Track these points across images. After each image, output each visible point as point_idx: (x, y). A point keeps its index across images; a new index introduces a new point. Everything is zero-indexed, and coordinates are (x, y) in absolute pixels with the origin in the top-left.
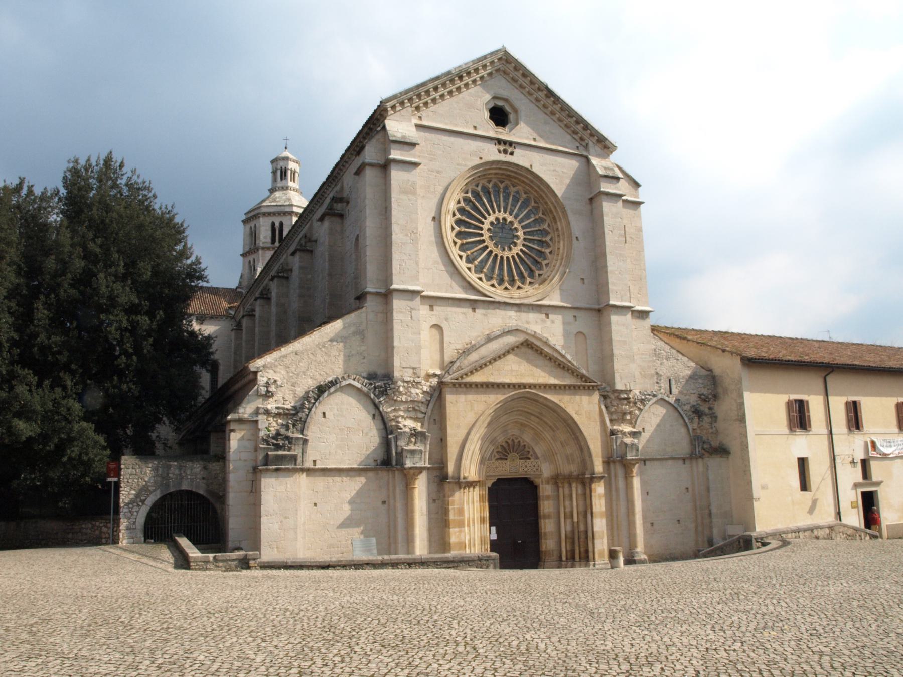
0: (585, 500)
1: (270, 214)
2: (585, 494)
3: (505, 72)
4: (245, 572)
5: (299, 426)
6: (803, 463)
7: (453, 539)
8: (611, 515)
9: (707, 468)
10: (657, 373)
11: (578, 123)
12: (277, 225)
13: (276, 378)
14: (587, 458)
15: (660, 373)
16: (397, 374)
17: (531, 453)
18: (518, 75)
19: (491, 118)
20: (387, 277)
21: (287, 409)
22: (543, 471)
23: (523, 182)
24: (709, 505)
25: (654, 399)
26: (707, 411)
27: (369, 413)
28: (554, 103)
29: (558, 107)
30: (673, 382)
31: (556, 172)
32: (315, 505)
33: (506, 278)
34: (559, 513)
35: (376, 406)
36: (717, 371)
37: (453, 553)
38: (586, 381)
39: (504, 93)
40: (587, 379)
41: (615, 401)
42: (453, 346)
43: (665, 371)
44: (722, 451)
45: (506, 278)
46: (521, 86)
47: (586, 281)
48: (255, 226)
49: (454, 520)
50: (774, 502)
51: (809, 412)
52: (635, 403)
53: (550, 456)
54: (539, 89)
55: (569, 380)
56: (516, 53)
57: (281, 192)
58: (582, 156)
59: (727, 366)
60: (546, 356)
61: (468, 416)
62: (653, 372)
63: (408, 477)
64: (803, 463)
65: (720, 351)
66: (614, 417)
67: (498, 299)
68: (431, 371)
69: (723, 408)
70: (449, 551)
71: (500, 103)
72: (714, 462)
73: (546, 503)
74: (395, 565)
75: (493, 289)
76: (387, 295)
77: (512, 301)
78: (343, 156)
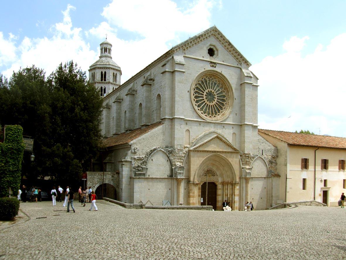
0: (232, 190)
1: (100, 68)
2: (232, 188)
3: (215, 35)
4: (142, 209)
5: (145, 164)
6: (304, 180)
7: (191, 202)
8: (240, 196)
9: (272, 181)
10: (259, 148)
11: (239, 55)
12: (103, 73)
13: (137, 147)
14: (234, 176)
15: (260, 148)
16: (175, 147)
17: (216, 174)
18: (219, 36)
19: (209, 53)
20: (172, 112)
21: (141, 158)
22: (219, 180)
23: (218, 77)
24: (272, 194)
25: (257, 157)
26: (274, 161)
27: (166, 160)
28: (231, 47)
29: (232, 49)
30: (264, 151)
31: (231, 76)
32: (149, 189)
33: (210, 113)
34: (223, 194)
35: (168, 157)
36: (279, 148)
37: (191, 206)
38: (235, 150)
39: (214, 43)
40: (234, 149)
41: (246, 158)
42: (193, 137)
43: (261, 147)
44: (278, 176)
45: (210, 113)
46: (220, 41)
47: (237, 115)
48: (94, 73)
49: (192, 195)
50: (294, 193)
51: (308, 163)
52: (251, 158)
53: (222, 175)
54: (226, 42)
55: (230, 150)
56: (219, 28)
57: (105, 58)
58: (239, 68)
59: (283, 146)
60: (223, 141)
61: (197, 162)
62: (257, 147)
63: (179, 181)
64: (304, 180)
65: (281, 141)
66: (244, 163)
67: (208, 121)
68: (186, 146)
69: (280, 160)
70: (190, 205)
71: (212, 47)
72: (275, 179)
73: (219, 191)
74: (173, 208)
75: (206, 117)
76: (172, 120)
77: (213, 122)
78: (153, 63)
